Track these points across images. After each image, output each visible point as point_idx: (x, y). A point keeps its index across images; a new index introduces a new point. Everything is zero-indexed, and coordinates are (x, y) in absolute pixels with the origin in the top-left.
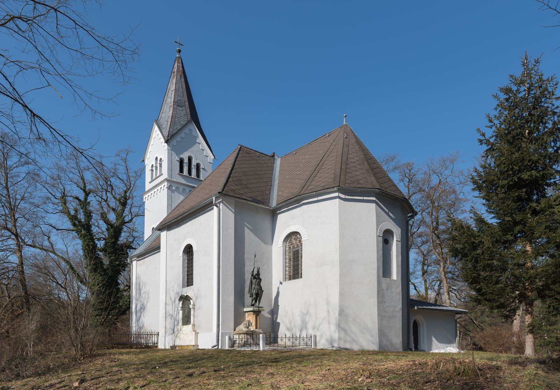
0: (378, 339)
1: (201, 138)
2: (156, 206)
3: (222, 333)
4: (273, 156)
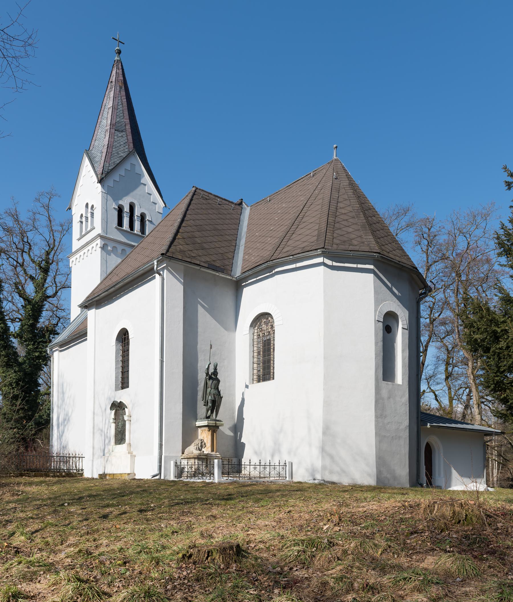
0: (375, 470)
2: (86, 270)
3: (165, 457)
4: (241, 204)
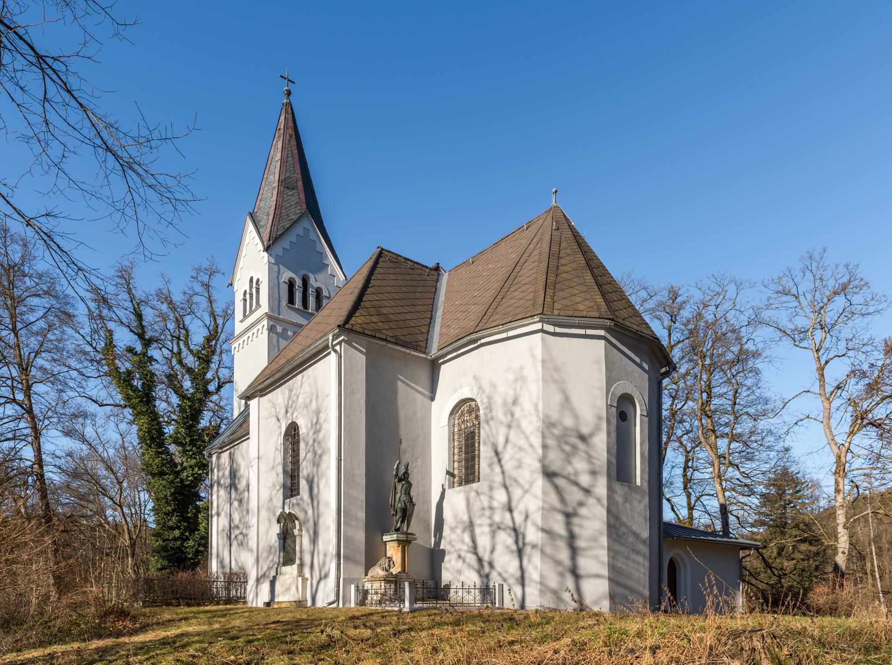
2: (249, 355)
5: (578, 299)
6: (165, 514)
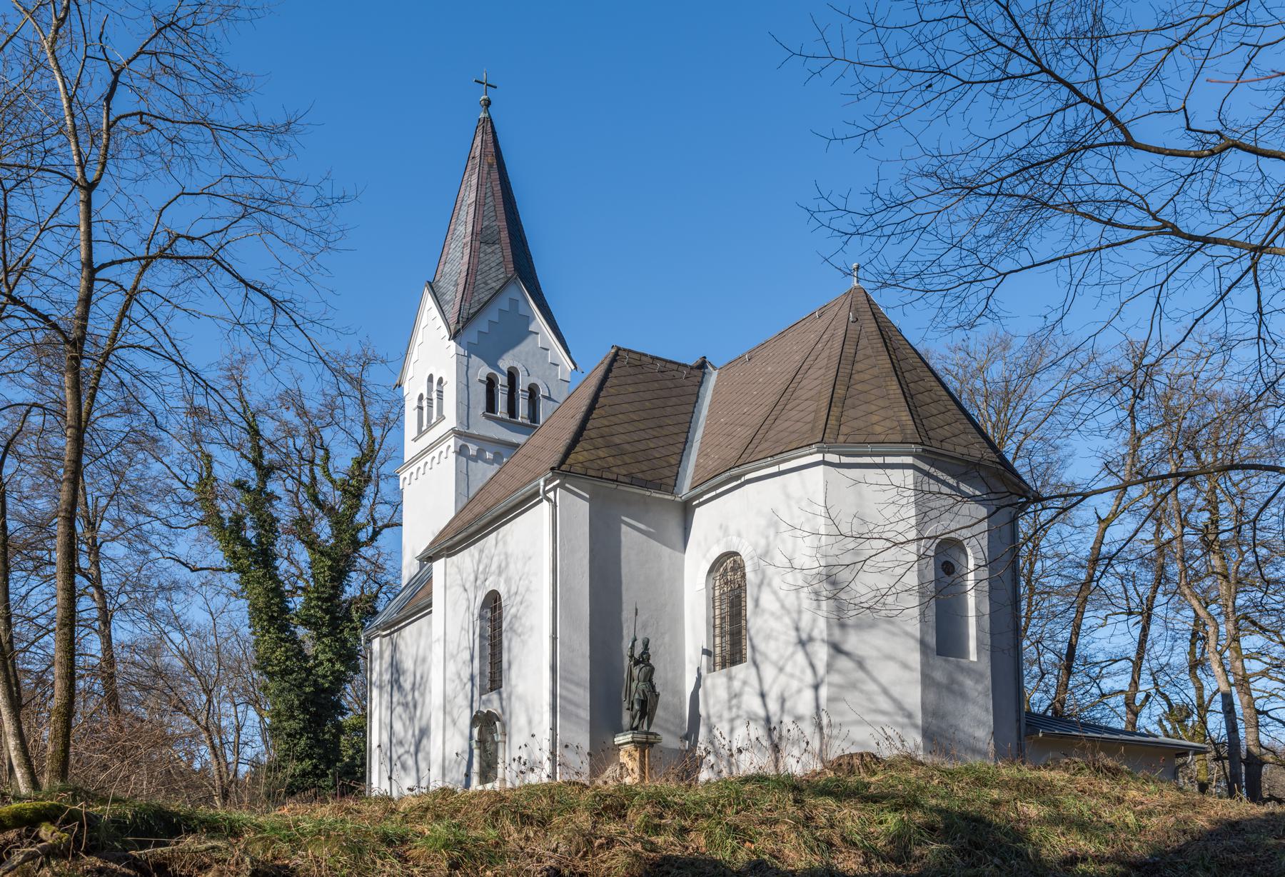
1: (540, 322)
2: (427, 494)
5: (875, 418)
6: (289, 735)
